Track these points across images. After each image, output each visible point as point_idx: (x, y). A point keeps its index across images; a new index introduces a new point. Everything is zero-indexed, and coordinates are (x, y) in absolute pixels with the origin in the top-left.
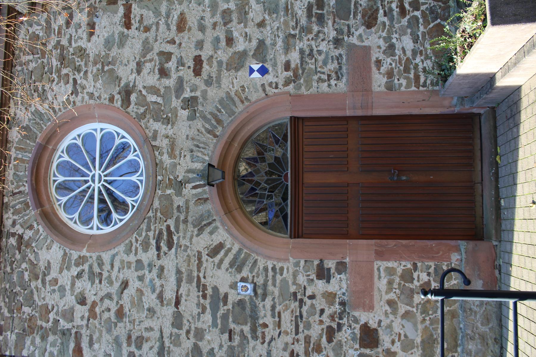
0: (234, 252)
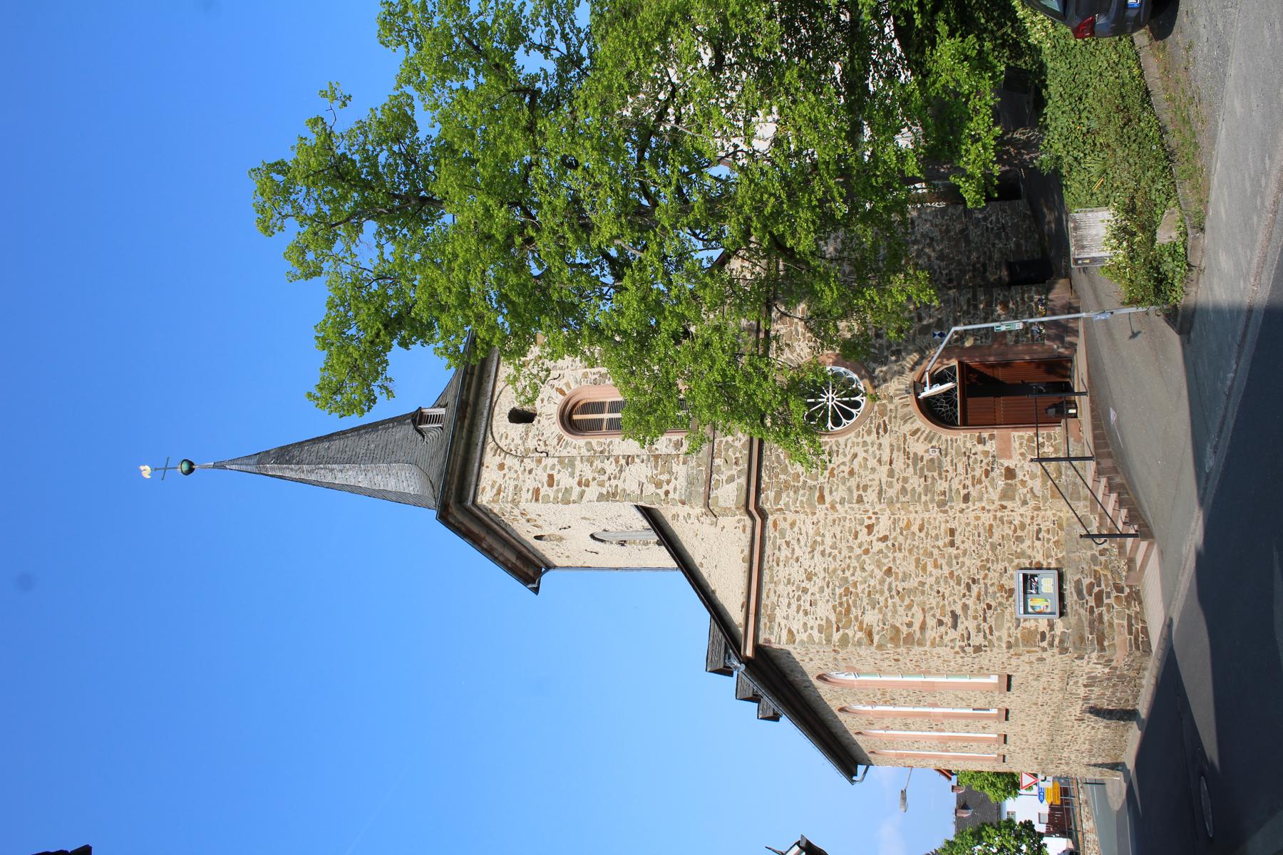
0: (927, 432)
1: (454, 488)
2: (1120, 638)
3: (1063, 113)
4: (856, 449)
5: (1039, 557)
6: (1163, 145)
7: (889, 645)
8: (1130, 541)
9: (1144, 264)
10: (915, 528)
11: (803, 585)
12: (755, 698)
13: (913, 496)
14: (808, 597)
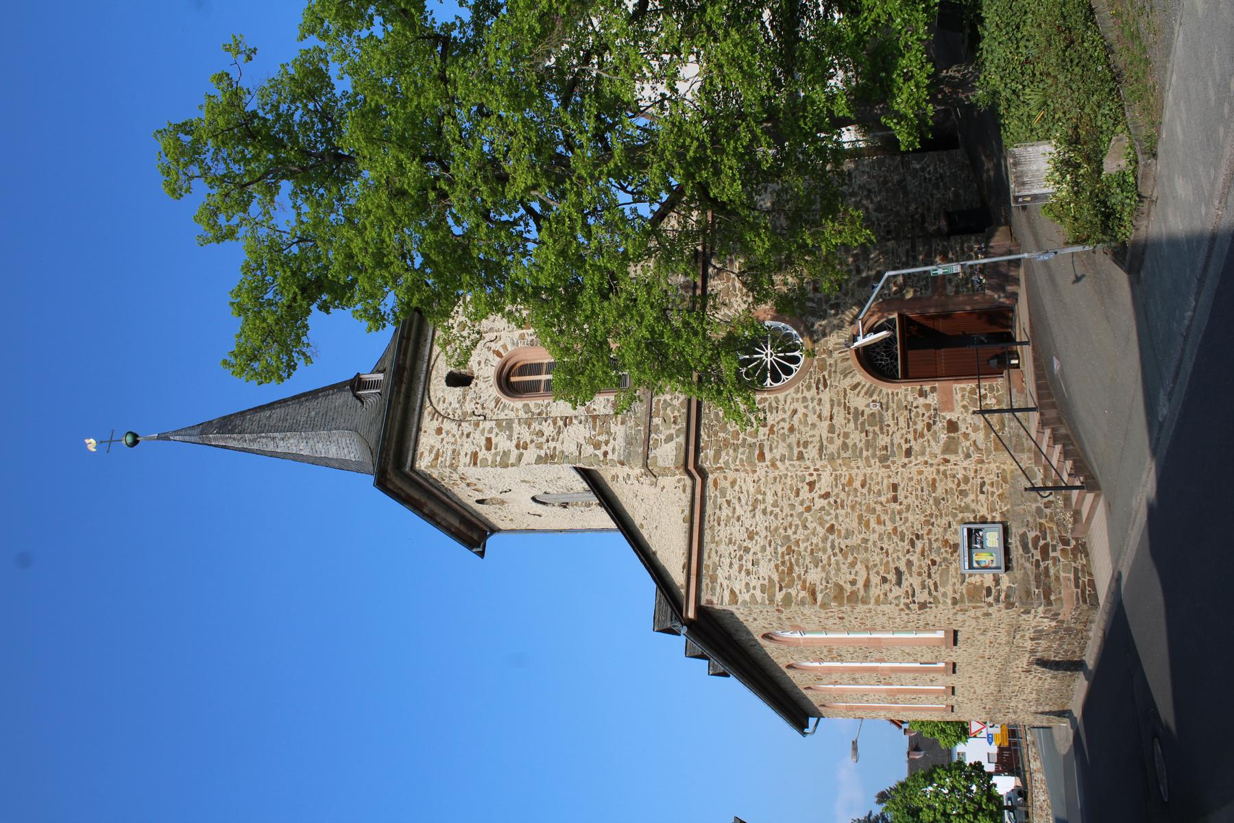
0: (867, 386)
1: (391, 454)
2: (1067, 592)
3: (1000, 43)
4: (795, 405)
5: (983, 511)
6: (1109, 66)
7: (833, 604)
8: (1075, 493)
9: (1090, 198)
10: (857, 484)
11: (745, 544)
12: (702, 657)
13: (854, 451)
14: (750, 556)
